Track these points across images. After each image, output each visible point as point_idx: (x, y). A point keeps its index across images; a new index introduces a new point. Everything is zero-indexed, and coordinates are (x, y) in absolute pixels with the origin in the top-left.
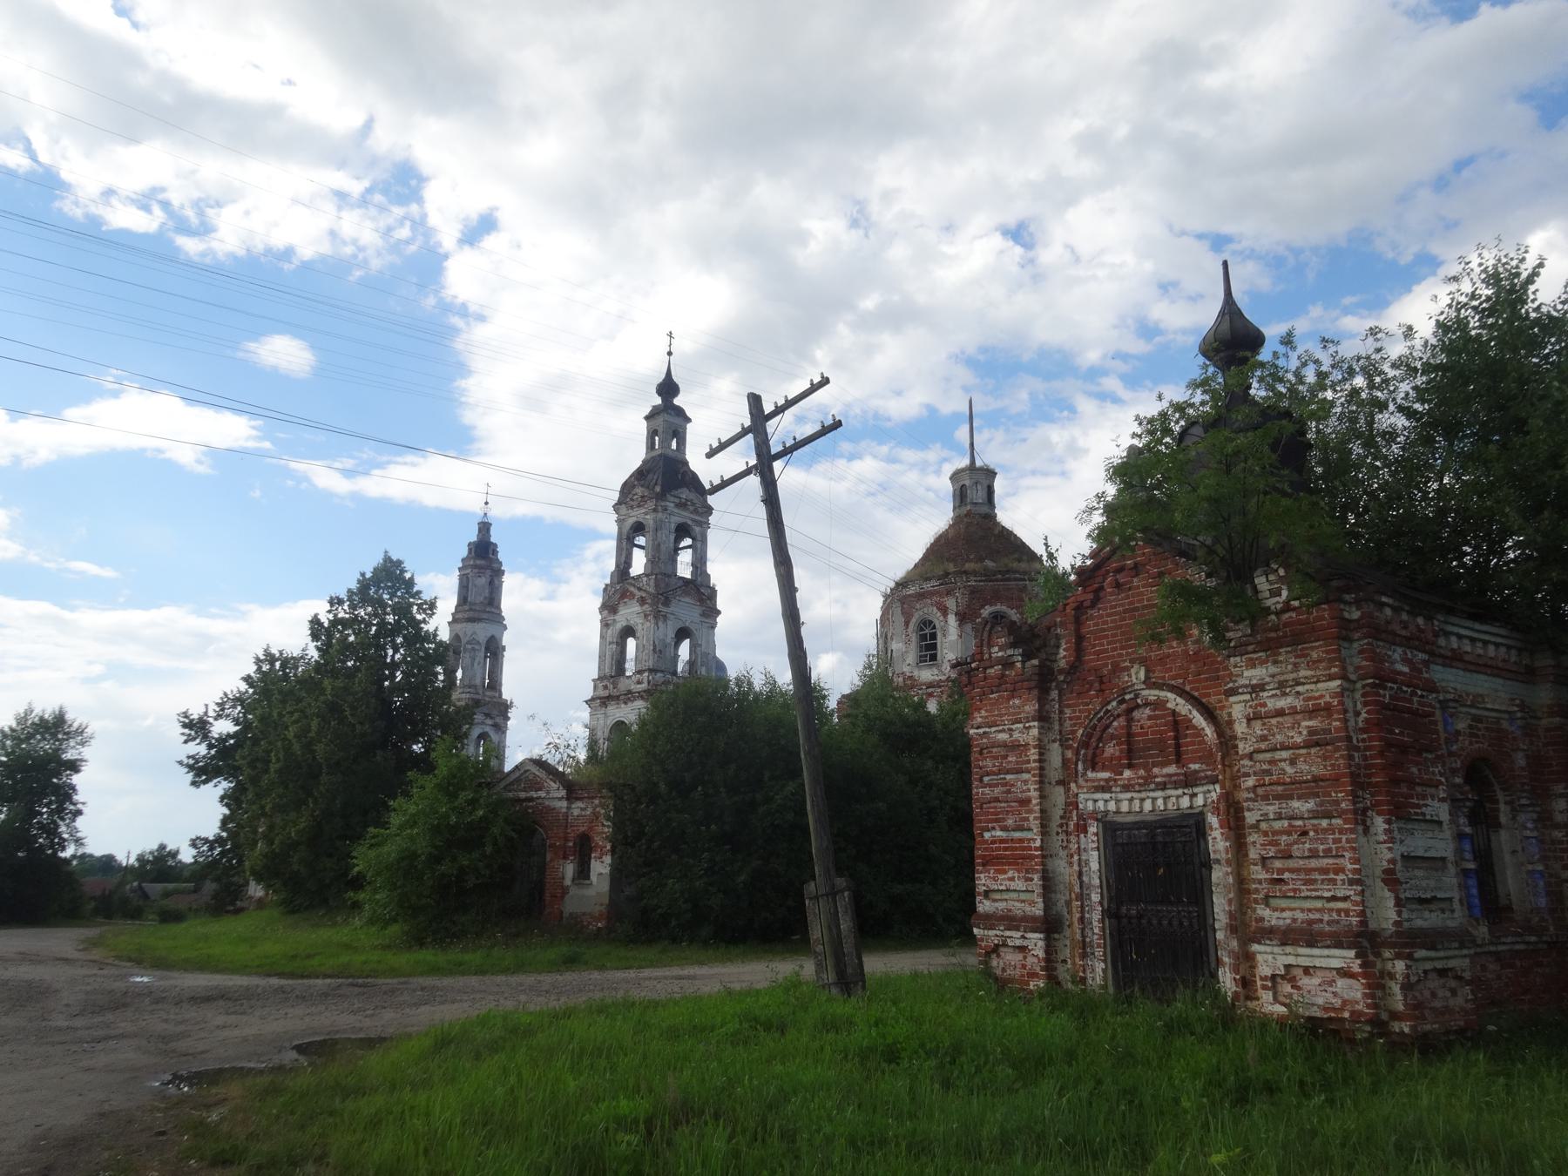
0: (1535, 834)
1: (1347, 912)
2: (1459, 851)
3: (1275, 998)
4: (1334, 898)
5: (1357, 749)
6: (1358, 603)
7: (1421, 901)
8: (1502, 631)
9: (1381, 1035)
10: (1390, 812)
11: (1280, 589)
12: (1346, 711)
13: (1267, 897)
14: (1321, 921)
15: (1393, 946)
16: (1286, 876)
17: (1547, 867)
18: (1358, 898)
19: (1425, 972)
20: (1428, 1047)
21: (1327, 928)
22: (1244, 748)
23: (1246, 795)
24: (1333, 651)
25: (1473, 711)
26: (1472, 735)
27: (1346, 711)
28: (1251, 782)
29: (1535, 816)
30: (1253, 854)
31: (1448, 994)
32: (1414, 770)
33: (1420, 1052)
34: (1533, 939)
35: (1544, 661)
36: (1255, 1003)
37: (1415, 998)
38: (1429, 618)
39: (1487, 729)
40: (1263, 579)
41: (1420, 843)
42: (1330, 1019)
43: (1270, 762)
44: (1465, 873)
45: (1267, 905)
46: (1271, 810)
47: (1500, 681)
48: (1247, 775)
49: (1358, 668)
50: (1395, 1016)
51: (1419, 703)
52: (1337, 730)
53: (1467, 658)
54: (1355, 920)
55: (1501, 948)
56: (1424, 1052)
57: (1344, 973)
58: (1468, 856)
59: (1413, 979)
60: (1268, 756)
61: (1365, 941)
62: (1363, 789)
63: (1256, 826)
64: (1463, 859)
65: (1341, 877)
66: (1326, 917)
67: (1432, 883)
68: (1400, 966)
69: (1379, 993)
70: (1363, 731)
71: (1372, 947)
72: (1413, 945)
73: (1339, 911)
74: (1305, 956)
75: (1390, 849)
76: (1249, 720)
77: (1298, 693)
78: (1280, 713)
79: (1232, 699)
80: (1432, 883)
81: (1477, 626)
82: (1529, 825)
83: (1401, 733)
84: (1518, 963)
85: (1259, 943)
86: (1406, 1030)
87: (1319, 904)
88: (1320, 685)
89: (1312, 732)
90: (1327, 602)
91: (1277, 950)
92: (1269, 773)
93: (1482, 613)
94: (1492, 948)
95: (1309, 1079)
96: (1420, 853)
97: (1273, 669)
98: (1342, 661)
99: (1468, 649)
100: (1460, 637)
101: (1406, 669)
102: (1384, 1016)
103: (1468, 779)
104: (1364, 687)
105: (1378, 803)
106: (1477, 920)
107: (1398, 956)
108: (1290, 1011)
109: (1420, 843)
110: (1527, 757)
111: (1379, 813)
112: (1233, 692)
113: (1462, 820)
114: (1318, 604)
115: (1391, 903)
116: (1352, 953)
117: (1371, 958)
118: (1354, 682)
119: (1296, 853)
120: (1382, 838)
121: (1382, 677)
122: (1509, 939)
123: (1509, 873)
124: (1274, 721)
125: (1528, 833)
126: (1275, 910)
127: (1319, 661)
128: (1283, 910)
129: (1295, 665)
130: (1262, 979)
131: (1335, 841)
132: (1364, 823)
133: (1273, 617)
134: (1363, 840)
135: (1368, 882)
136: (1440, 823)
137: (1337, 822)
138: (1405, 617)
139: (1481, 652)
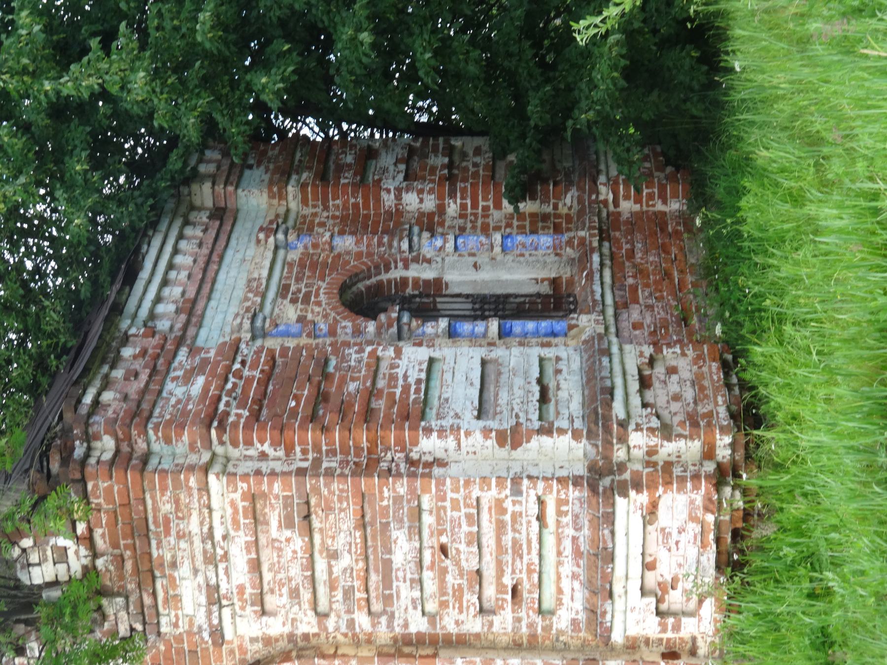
0: (451, 238)
1: (560, 502)
2: (474, 339)
3: (692, 614)
4: (541, 518)
5: (317, 462)
6: (89, 438)
7: (544, 398)
8: (156, 242)
9: (737, 475)
10: (414, 428)
11: (55, 548)
12: (258, 473)
13: (540, 611)
14: (575, 539)
15: (608, 444)
16: (508, 581)
17: (497, 228)
18: (541, 485)
19: (645, 405)
20: (749, 415)
21: (586, 531)
22: (308, 625)
23: (383, 628)
24: (163, 480)
25: (271, 295)
26: (306, 300)
27: (258, 473)
28: (363, 621)
29: (426, 235)
30: (474, 625)
31: (674, 378)
32: (352, 387)
33: (757, 428)
34: (596, 258)
35: (204, 194)
36: (700, 643)
37: (682, 424)
38: (126, 340)
39: (298, 280)
40: (36, 572)
41: (458, 388)
42: (718, 540)
43: (332, 588)
44: (503, 334)
45: (552, 613)
46: (406, 593)
47: (230, 253)
48: (351, 623)
49: (192, 447)
50: (709, 453)
51: (254, 366)
52: (286, 486)
53: (191, 293)
54: (573, 493)
55: (609, 300)
56: (757, 422)
57: (651, 512)
58: (480, 327)
59: (655, 423)
60: (322, 590)
61: (603, 481)
62: (378, 461)
63: (432, 619)
64: (485, 335)
65: (508, 504)
66: (570, 532)
67: (519, 381)
68: (638, 440)
69: (677, 471)
70: (289, 450)
71: (611, 472)
72: (607, 419)
73: (560, 513)
74: (626, 570)
75: (468, 434)
76: (264, 613)
77: (225, 537)
78: (256, 566)
79: (229, 635)
80: (519, 381)
81: (144, 275)
82: (439, 242)
83: (297, 398)
84: (630, 281)
85: (610, 630)
86: (728, 440)
87: (550, 540)
88: (215, 504)
89: (288, 523)
90: (83, 481)
91: (619, 603)
92: (348, 593)
93: (126, 265)
94: (610, 311)
95: (806, 585)
96: (475, 393)
97: (185, 570)
98: (179, 469)
99: (177, 291)
100: (158, 299)
101: (201, 381)
102: (710, 467)
103: (371, 313)
104: (222, 443)
105: (400, 442)
106: (571, 327)
107: (623, 439)
108: (710, 594)
109: (458, 388)
110: (342, 233)
111: (415, 443)
112: (217, 634)
113: (429, 328)
114: (85, 496)
115: (545, 440)
116: (620, 501)
117: (627, 476)
118: (214, 455)
119: (474, 565)
120: (451, 442)
121: (212, 417)
122: (597, 288)
123: (505, 276)
124: (267, 576)
125: (450, 246)
126: (559, 602)
127: (177, 502)
128: (560, 591)
129: (180, 536)
130: (664, 630)
131: (456, 506)
132: (429, 465)
133: (100, 563)
134: (453, 469)
135: (516, 468)
136: (431, 361)
137: (427, 502)
138: (118, 374)
139: (184, 275)
